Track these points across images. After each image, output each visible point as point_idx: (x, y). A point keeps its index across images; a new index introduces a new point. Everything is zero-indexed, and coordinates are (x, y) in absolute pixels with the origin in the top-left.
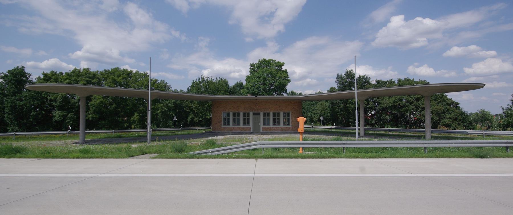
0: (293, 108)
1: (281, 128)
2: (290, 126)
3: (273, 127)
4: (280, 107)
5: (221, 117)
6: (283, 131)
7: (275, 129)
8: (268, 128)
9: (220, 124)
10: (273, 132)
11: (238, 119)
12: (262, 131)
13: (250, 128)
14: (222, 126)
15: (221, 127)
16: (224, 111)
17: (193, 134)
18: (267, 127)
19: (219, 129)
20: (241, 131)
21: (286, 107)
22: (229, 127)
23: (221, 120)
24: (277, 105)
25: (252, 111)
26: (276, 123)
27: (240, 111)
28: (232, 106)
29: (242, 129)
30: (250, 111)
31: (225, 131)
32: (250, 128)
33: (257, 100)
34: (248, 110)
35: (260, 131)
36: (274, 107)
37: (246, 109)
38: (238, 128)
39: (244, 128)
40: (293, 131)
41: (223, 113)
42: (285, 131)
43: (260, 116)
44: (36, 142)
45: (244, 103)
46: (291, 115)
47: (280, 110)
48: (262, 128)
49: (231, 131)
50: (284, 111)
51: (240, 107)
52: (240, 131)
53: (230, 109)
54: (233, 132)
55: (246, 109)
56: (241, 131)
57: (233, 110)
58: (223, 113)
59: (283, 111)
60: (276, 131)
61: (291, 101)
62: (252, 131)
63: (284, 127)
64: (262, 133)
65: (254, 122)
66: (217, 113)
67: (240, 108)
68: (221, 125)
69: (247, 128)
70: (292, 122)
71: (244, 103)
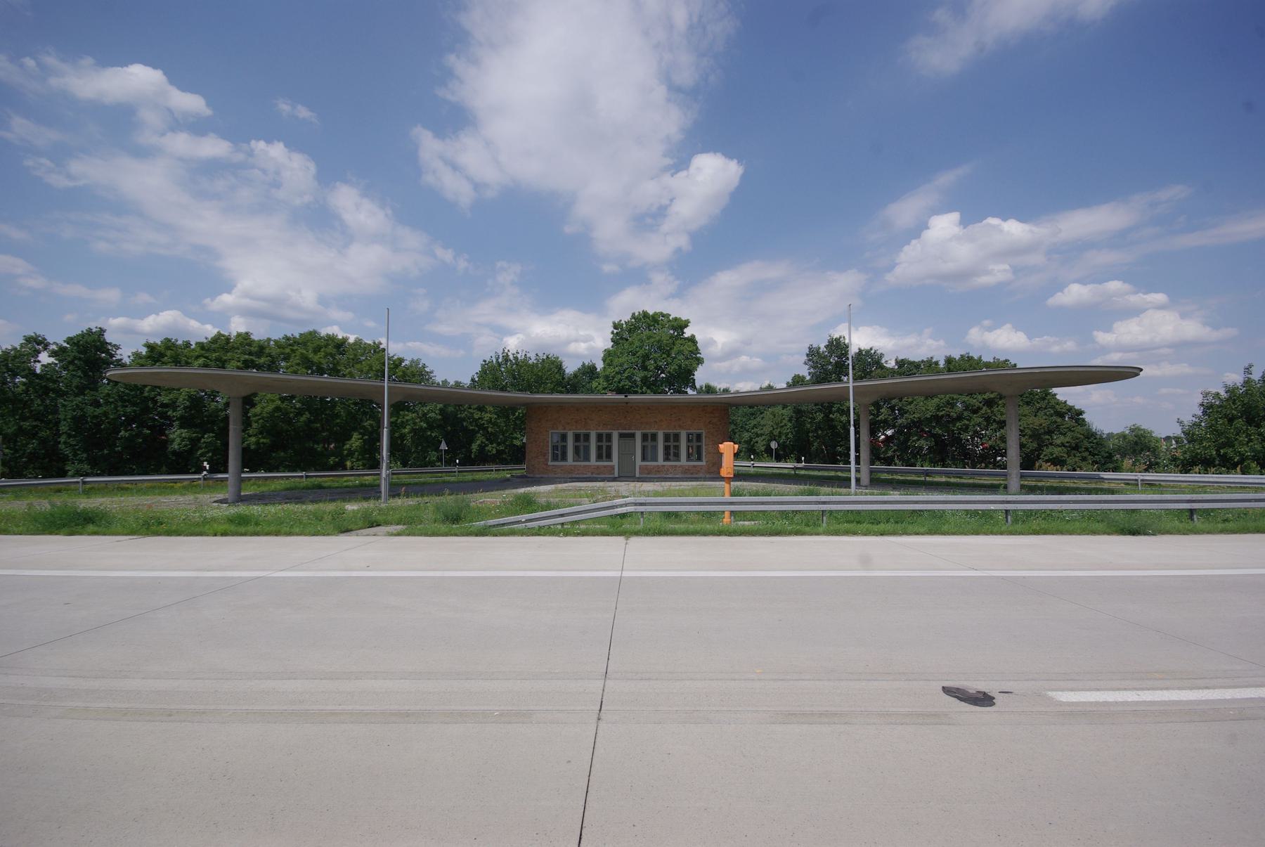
1: (681, 466)
2: (704, 463)
3: (664, 466)
5: (548, 442)
14: (550, 463)
16: (553, 428)
17: (483, 481)
20: (592, 473)
32: (612, 468)
33: (629, 404)
34: (609, 427)
35: (635, 476)
38: (585, 466)
39: (598, 467)
40: (710, 473)
44: (130, 499)
47: (680, 427)
49: (569, 473)
54: (574, 476)
55: (604, 424)
56: (592, 473)
60: (671, 473)
61: (704, 406)
63: (689, 466)
64: (638, 478)
68: (547, 460)
69: (605, 467)
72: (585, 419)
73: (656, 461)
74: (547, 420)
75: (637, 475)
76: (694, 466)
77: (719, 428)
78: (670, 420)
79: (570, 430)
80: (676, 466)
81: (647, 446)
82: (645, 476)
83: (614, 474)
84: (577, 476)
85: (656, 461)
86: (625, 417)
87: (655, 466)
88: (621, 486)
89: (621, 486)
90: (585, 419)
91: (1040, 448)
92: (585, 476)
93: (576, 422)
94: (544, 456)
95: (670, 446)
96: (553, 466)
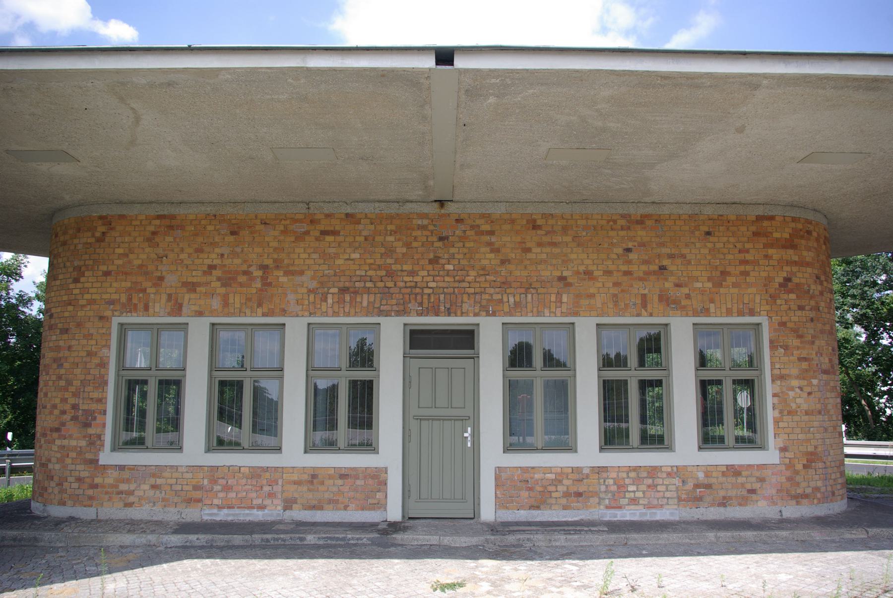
0: (788, 280)
1: (677, 472)
2: (769, 456)
3: (604, 469)
4: (662, 268)
5: (103, 365)
6: (697, 500)
7: (621, 487)
8: (557, 481)
9: (91, 431)
10: (610, 515)
11: (644, 385)
12: (501, 504)
13: (378, 478)
14: (107, 457)
15: (94, 462)
16: (130, 307)
17: (524, 526)
18: (549, 470)
19: (79, 480)
20: (288, 504)
21: (724, 273)
22: (175, 468)
23: (101, 401)
24: (632, 256)
25: (401, 313)
26: (729, 429)
27: (284, 312)
28: (212, 267)
29: (298, 483)
30: (381, 313)
31: (130, 505)
32: (378, 478)
33: (451, 208)
34: (365, 300)
35: (476, 515)
36: (608, 273)
37: (343, 290)
38: (256, 473)
39: (314, 477)
40: (798, 498)
41: (123, 328)
42: (724, 503)
43: (475, 358)
44: (665, 535)
45: (324, 233)
46: (773, 346)
47: (668, 302)
48: (497, 478)
49: (189, 501)
50: (706, 312)
51: (287, 273)
52: (273, 512)
53: (192, 287)
54: (209, 514)
55: (343, 290)
56: (288, 504)
57: (216, 303)
58: (123, 328)
59: (696, 314)
60: (634, 501)
61: (760, 218)
62: (394, 513)
63: (709, 470)
64: (494, 528)
65: (421, 419)
66: (65, 331)
67: (283, 279)
68: (95, 442)
69: (344, 475)
70: (786, 410)
71: (324, 233)
72: (264, 268)
73: (569, 447)
74: (107, 274)
75: (488, 512)
76: (734, 471)
77: (817, 308)
78: (627, 273)
79: (200, 314)
80: (653, 471)
81: (528, 386)
82: (523, 515)
83: (381, 506)
84: (223, 515)
85: (569, 447)
86: (434, 261)
87: (561, 475)
88: (108, 578)
89: (108, 578)
90: (264, 268)
91: (856, 417)
92: (258, 515)
93: (227, 281)
94: (87, 425)
95: (625, 382)
96: (122, 468)
